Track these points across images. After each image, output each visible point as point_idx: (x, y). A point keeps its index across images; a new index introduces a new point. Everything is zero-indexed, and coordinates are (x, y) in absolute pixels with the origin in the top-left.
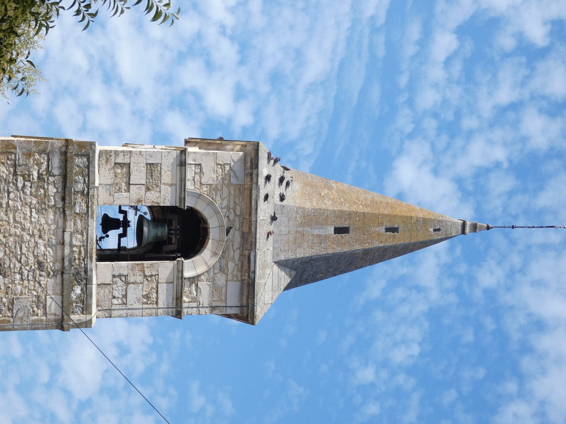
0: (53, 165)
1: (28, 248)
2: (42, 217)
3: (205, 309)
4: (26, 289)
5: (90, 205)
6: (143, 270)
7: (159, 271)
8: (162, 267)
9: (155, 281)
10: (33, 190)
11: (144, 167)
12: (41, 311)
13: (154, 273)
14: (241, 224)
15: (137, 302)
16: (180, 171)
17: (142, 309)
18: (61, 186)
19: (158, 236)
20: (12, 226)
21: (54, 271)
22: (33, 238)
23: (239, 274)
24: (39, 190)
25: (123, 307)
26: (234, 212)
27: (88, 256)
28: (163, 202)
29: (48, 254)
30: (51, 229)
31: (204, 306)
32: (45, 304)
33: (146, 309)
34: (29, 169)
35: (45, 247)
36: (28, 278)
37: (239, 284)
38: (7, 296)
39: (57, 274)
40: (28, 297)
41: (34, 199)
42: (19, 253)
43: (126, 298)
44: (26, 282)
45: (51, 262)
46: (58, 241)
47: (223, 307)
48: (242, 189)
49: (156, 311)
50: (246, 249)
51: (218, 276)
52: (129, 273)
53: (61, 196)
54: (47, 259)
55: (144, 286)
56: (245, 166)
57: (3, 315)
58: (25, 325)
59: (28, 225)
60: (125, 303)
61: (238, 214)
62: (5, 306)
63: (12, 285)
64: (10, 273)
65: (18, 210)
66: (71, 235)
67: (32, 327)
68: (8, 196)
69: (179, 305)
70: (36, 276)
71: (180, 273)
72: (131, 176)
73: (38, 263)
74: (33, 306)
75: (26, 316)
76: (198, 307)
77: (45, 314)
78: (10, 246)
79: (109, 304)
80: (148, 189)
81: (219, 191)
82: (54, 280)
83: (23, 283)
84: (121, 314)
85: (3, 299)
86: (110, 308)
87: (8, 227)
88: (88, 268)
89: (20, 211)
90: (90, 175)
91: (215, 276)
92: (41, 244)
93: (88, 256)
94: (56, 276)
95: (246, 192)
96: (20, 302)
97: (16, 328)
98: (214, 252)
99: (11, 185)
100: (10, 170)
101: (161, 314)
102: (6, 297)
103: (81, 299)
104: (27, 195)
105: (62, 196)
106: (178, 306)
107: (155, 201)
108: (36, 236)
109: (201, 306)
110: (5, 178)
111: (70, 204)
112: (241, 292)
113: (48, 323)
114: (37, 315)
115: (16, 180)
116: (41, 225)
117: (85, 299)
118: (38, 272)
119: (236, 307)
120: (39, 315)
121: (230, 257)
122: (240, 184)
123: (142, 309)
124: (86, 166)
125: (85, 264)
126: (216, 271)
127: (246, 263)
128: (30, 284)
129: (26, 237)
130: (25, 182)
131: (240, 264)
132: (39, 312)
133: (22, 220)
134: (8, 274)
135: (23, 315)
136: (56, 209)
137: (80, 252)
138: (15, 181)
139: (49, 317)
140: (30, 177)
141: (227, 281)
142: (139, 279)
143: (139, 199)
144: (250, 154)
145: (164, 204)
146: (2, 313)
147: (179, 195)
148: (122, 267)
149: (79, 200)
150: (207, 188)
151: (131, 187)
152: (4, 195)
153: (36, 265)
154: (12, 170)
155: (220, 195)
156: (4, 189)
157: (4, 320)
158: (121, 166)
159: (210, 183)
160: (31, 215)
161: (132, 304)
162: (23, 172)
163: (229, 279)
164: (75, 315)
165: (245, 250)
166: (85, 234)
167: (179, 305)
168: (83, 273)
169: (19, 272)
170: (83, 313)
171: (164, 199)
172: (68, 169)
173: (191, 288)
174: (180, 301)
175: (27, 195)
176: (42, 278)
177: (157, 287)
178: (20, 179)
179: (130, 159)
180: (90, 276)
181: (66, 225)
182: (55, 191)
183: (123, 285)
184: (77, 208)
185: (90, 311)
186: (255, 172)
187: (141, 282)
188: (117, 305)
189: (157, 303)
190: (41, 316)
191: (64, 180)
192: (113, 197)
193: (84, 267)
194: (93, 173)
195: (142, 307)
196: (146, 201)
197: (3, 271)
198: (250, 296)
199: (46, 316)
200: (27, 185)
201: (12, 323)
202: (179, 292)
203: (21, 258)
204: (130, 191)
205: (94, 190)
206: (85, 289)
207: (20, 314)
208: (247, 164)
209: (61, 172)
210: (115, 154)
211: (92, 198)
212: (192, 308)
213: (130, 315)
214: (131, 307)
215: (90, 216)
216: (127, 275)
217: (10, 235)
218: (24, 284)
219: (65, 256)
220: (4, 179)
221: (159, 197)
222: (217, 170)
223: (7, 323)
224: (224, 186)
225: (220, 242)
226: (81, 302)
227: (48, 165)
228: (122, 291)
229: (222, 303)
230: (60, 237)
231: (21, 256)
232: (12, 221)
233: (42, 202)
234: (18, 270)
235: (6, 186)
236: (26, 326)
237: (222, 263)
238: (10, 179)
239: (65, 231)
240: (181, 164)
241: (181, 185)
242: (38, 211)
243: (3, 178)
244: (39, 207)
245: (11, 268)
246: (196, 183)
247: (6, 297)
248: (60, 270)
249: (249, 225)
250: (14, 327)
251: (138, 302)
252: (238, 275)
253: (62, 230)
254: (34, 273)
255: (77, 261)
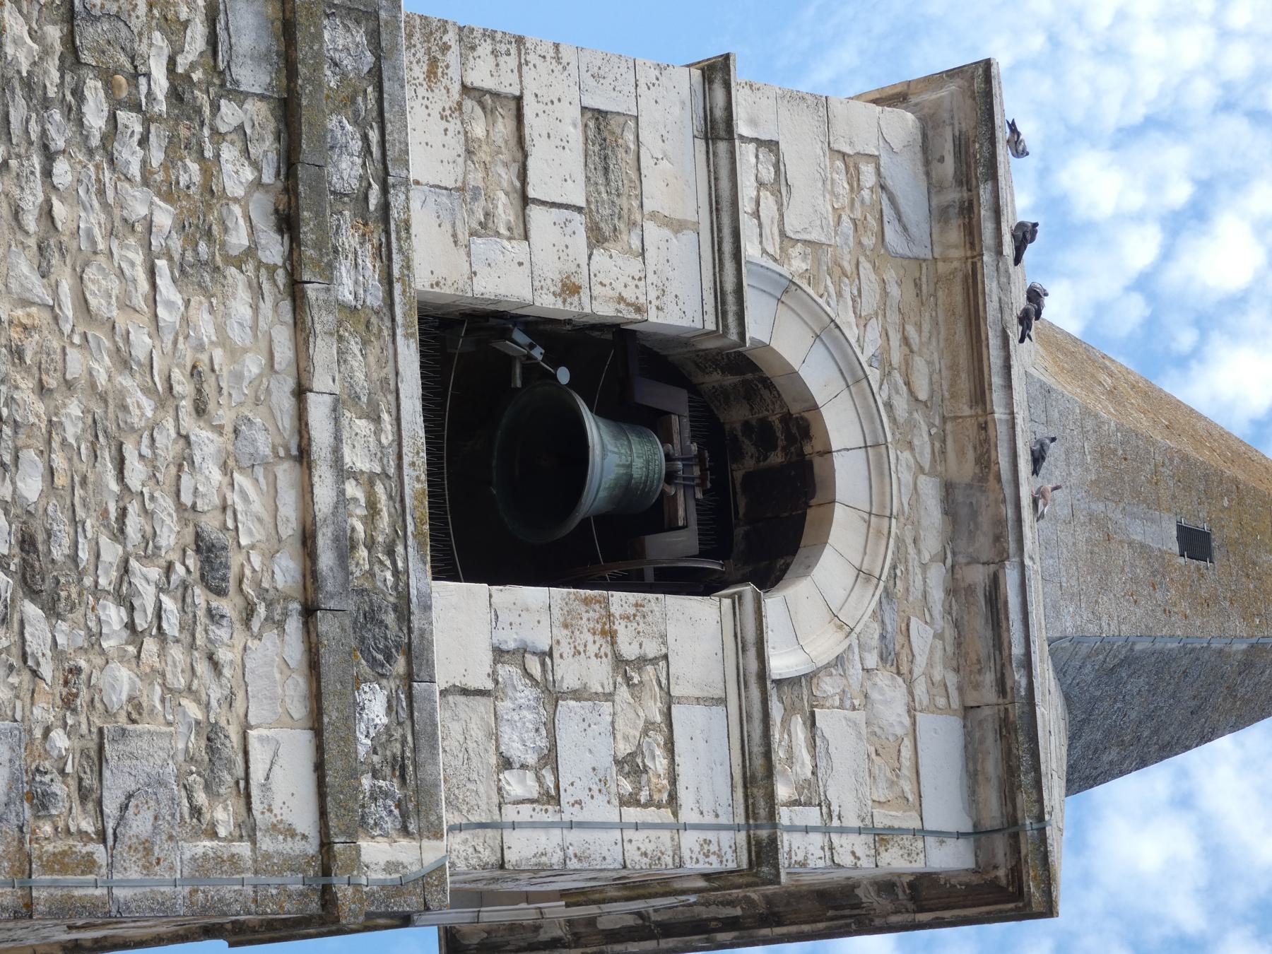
0: (233, 41)
1: (152, 464)
2: (201, 303)
3: (853, 837)
4: (151, 684)
5: (396, 272)
6: (607, 627)
7: (670, 641)
8: (678, 620)
9: (657, 689)
10: (157, 157)
11: (575, 126)
12: (225, 809)
13: (652, 649)
14: (937, 445)
15: (600, 791)
16: (708, 166)
17: (622, 826)
18: (272, 156)
19: (631, 476)
20: (70, 337)
21: (268, 597)
22: (172, 412)
23: (952, 679)
24: (181, 159)
25: (548, 814)
26: (907, 384)
27: (410, 528)
28: (658, 303)
29: (239, 507)
30: (246, 374)
31: (846, 823)
32: (240, 772)
33: (636, 827)
34: (132, 41)
35: (224, 467)
36: (160, 628)
37: (955, 723)
38: (70, 722)
39: (286, 614)
40: (165, 729)
41: (162, 204)
42: (114, 486)
43: (556, 771)
44: (150, 645)
45: (253, 547)
46: (278, 440)
47: (914, 832)
48: (924, 279)
49: (673, 839)
50: (973, 561)
51: (879, 683)
52: (558, 642)
53: (271, 208)
54: (237, 528)
55: (618, 709)
56: (928, 174)
57: (56, 829)
58: (162, 883)
59: (141, 342)
60: (553, 792)
61: (923, 396)
62: (62, 772)
63: (89, 661)
64: (80, 594)
65: (95, 253)
66: (334, 410)
67: (194, 899)
68: (48, 173)
69: (763, 813)
70: (195, 616)
71: (752, 653)
72: (531, 163)
73: (198, 550)
74: (191, 778)
75: (164, 837)
76: (826, 830)
77: (247, 829)
78: (71, 445)
79: (489, 798)
80: (597, 238)
81: (846, 280)
82: (274, 644)
83: (139, 652)
84: (541, 850)
85: (53, 734)
86: (497, 817)
87: (56, 344)
88: (413, 592)
89: (102, 259)
90: (386, 115)
91: (868, 684)
92: (205, 448)
93: (409, 533)
94: (280, 625)
95: (940, 293)
96: (132, 756)
97: (122, 900)
98: (857, 565)
99: (57, 115)
100: (43, 37)
101: (694, 857)
102: (65, 725)
103: (394, 757)
104: (129, 180)
105: (276, 211)
106: (755, 820)
107: (629, 295)
108: (183, 403)
109: (836, 823)
110: (25, 74)
111: (320, 250)
112: (967, 767)
113: (263, 878)
114: (214, 835)
115: (78, 93)
116: (200, 347)
117: (408, 754)
118: (200, 596)
119: (959, 835)
120: (222, 832)
121: (911, 599)
122: (917, 259)
123: (622, 826)
124: (366, 69)
125: (396, 573)
126: (872, 660)
127: (978, 623)
128: (170, 662)
129: (139, 406)
130: (118, 112)
131: (950, 633)
132: (220, 814)
133: (115, 313)
134: (69, 596)
135: (149, 828)
136: (257, 269)
137: (372, 506)
138: (69, 97)
139: (266, 844)
140: (137, 87)
141: (911, 711)
142: (599, 674)
143: (568, 277)
144: (952, 117)
145: (660, 313)
146: (54, 812)
147: (711, 278)
148: (527, 610)
149: (349, 238)
150: (804, 257)
151: (535, 212)
152: (26, 163)
153: (192, 560)
154: (54, 33)
155: (854, 301)
156: (27, 132)
157: (64, 853)
158: (483, 108)
159: (814, 236)
160: (154, 286)
161: (579, 802)
162: (103, 52)
163: (920, 703)
164: (373, 837)
165: (968, 564)
166: (385, 416)
167: (763, 813)
168: (390, 619)
169: (118, 590)
170: (405, 831)
171: (660, 293)
172: (302, 70)
173: (790, 736)
174: (762, 792)
175: (129, 180)
176: (222, 633)
177: (668, 716)
178: (94, 89)
179: (521, 76)
180: (422, 632)
181: (309, 359)
182: (251, 177)
183: (538, 699)
184: (345, 280)
185: (433, 818)
186: (985, 193)
187: (607, 691)
188: (522, 802)
189: (673, 798)
190: (230, 839)
191: (282, 127)
192: (469, 254)
193: (395, 587)
194: (397, 108)
195: (618, 820)
196: (595, 293)
197: (43, 580)
198: (1022, 778)
199: (253, 841)
200: (126, 127)
201: (104, 870)
202: (757, 749)
203: (123, 512)
204: (533, 234)
205: (407, 198)
206: (404, 704)
207: (140, 824)
208: (935, 164)
209: (268, 80)
210: (461, 40)
211: (403, 234)
212: (806, 830)
213: (576, 856)
214: (579, 816)
215: (403, 325)
216: (551, 648)
217: (69, 385)
218: (142, 655)
219: (320, 516)
220: (21, 78)
221: (640, 279)
222: (833, 180)
223: (83, 873)
224: (862, 259)
225: (873, 519)
226: (393, 769)
227: (212, 40)
228: (537, 730)
229: (908, 813)
230: (287, 422)
231: (121, 504)
232: (68, 310)
233: (197, 227)
234: (113, 578)
235: (34, 115)
236: (167, 889)
237: (887, 621)
238: (48, 85)
239: (311, 391)
240: (712, 128)
241: (716, 229)
242: (182, 271)
243: (19, 72)
244: (184, 250)
245: (81, 567)
246: (766, 231)
247: (65, 725)
248: (296, 595)
249: (975, 448)
250: (115, 891)
251: (604, 791)
252: (948, 684)
253: (290, 384)
254: (184, 600)
255: (363, 553)
